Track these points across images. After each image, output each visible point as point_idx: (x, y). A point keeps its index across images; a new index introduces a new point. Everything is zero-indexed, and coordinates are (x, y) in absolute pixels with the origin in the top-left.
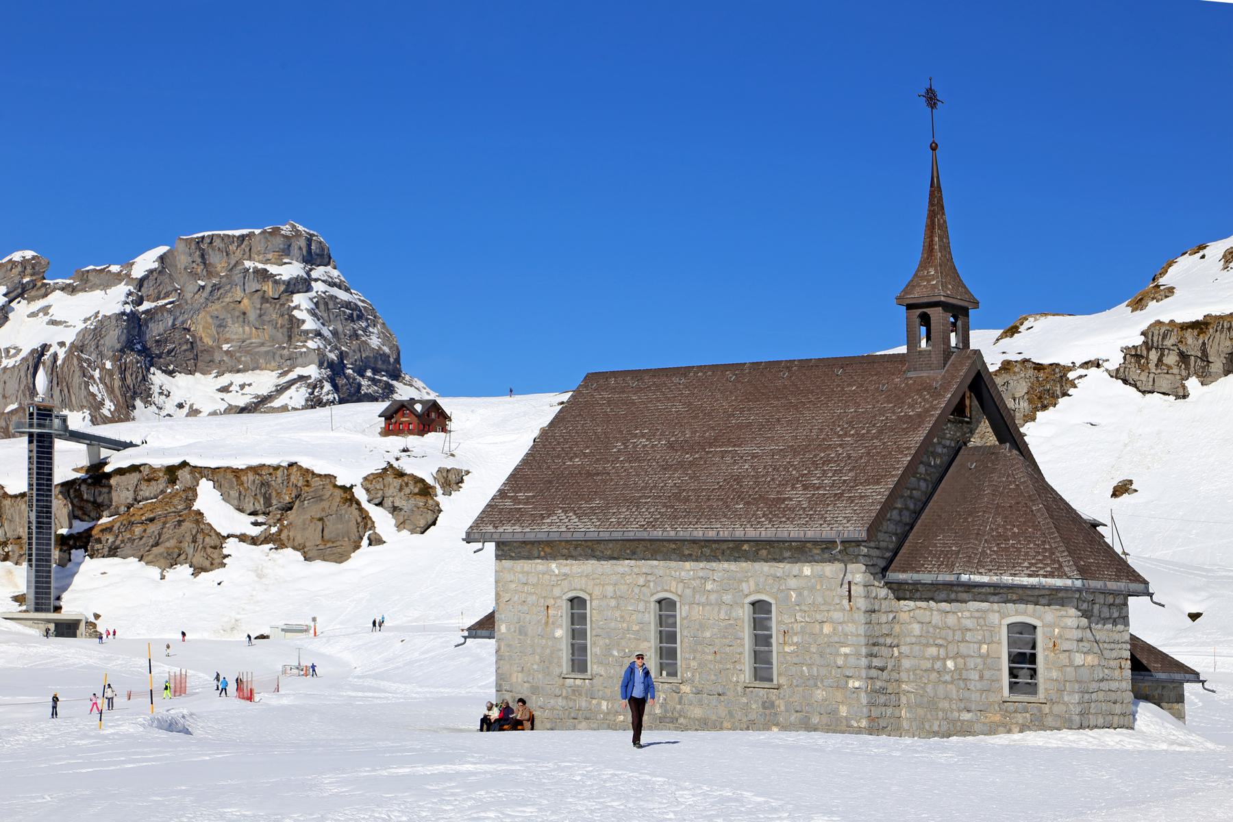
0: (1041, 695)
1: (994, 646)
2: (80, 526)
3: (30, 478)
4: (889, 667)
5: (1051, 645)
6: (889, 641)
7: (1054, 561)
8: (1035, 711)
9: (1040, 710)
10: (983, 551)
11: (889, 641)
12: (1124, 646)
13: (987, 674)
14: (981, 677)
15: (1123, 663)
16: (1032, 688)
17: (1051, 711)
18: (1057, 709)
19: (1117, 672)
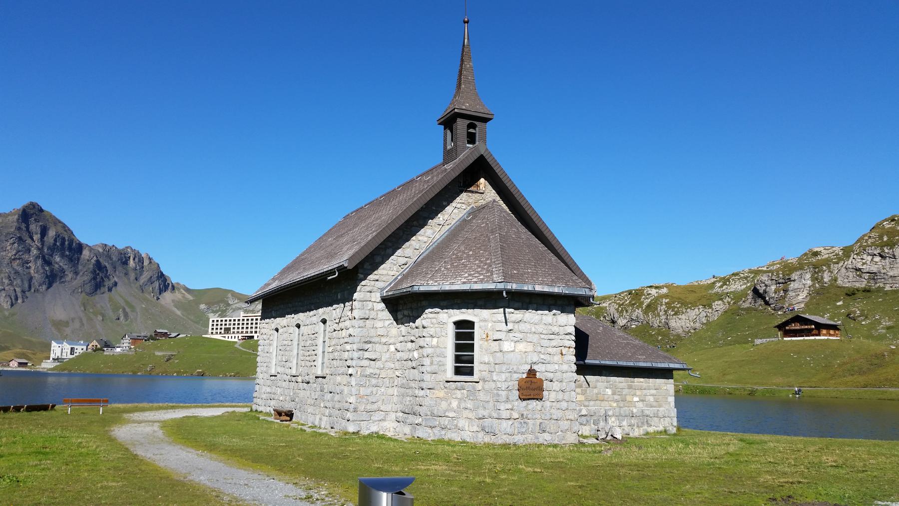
0: (476, 377)
1: (442, 339)
2: (435, 363)
3: (199, 407)
4: (383, 359)
5: (485, 336)
6: (384, 340)
7: (488, 271)
8: (470, 389)
9: (474, 388)
10: (440, 269)
11: (384, 340)
12: (568, 337)
13: (436, 359)
14: (432, 363)
15: (565, 351)
16: (470, 372)
17: (483, 388)
18: (489, 385)
19: (557, 358)
